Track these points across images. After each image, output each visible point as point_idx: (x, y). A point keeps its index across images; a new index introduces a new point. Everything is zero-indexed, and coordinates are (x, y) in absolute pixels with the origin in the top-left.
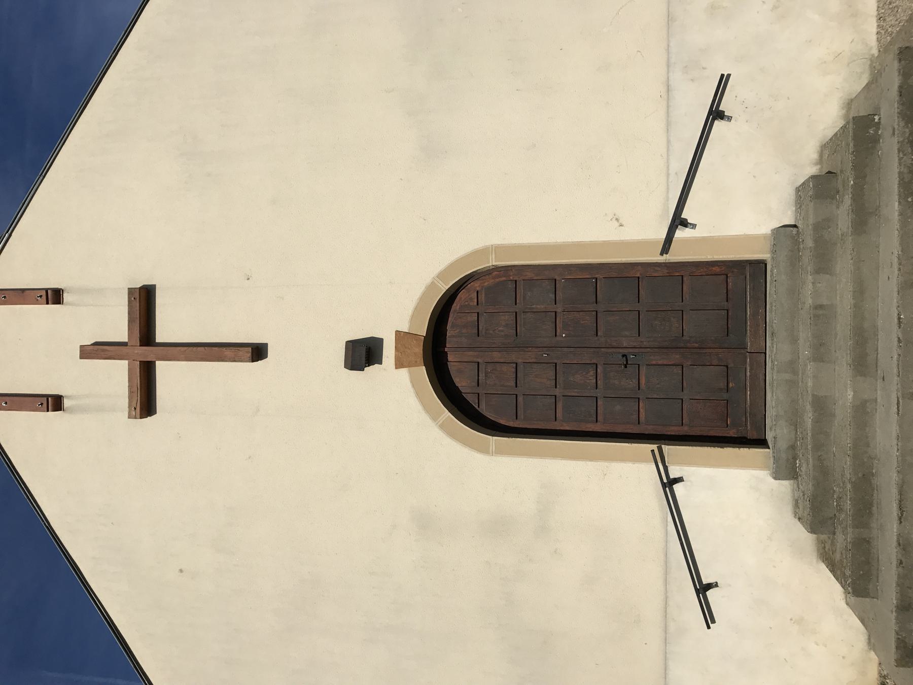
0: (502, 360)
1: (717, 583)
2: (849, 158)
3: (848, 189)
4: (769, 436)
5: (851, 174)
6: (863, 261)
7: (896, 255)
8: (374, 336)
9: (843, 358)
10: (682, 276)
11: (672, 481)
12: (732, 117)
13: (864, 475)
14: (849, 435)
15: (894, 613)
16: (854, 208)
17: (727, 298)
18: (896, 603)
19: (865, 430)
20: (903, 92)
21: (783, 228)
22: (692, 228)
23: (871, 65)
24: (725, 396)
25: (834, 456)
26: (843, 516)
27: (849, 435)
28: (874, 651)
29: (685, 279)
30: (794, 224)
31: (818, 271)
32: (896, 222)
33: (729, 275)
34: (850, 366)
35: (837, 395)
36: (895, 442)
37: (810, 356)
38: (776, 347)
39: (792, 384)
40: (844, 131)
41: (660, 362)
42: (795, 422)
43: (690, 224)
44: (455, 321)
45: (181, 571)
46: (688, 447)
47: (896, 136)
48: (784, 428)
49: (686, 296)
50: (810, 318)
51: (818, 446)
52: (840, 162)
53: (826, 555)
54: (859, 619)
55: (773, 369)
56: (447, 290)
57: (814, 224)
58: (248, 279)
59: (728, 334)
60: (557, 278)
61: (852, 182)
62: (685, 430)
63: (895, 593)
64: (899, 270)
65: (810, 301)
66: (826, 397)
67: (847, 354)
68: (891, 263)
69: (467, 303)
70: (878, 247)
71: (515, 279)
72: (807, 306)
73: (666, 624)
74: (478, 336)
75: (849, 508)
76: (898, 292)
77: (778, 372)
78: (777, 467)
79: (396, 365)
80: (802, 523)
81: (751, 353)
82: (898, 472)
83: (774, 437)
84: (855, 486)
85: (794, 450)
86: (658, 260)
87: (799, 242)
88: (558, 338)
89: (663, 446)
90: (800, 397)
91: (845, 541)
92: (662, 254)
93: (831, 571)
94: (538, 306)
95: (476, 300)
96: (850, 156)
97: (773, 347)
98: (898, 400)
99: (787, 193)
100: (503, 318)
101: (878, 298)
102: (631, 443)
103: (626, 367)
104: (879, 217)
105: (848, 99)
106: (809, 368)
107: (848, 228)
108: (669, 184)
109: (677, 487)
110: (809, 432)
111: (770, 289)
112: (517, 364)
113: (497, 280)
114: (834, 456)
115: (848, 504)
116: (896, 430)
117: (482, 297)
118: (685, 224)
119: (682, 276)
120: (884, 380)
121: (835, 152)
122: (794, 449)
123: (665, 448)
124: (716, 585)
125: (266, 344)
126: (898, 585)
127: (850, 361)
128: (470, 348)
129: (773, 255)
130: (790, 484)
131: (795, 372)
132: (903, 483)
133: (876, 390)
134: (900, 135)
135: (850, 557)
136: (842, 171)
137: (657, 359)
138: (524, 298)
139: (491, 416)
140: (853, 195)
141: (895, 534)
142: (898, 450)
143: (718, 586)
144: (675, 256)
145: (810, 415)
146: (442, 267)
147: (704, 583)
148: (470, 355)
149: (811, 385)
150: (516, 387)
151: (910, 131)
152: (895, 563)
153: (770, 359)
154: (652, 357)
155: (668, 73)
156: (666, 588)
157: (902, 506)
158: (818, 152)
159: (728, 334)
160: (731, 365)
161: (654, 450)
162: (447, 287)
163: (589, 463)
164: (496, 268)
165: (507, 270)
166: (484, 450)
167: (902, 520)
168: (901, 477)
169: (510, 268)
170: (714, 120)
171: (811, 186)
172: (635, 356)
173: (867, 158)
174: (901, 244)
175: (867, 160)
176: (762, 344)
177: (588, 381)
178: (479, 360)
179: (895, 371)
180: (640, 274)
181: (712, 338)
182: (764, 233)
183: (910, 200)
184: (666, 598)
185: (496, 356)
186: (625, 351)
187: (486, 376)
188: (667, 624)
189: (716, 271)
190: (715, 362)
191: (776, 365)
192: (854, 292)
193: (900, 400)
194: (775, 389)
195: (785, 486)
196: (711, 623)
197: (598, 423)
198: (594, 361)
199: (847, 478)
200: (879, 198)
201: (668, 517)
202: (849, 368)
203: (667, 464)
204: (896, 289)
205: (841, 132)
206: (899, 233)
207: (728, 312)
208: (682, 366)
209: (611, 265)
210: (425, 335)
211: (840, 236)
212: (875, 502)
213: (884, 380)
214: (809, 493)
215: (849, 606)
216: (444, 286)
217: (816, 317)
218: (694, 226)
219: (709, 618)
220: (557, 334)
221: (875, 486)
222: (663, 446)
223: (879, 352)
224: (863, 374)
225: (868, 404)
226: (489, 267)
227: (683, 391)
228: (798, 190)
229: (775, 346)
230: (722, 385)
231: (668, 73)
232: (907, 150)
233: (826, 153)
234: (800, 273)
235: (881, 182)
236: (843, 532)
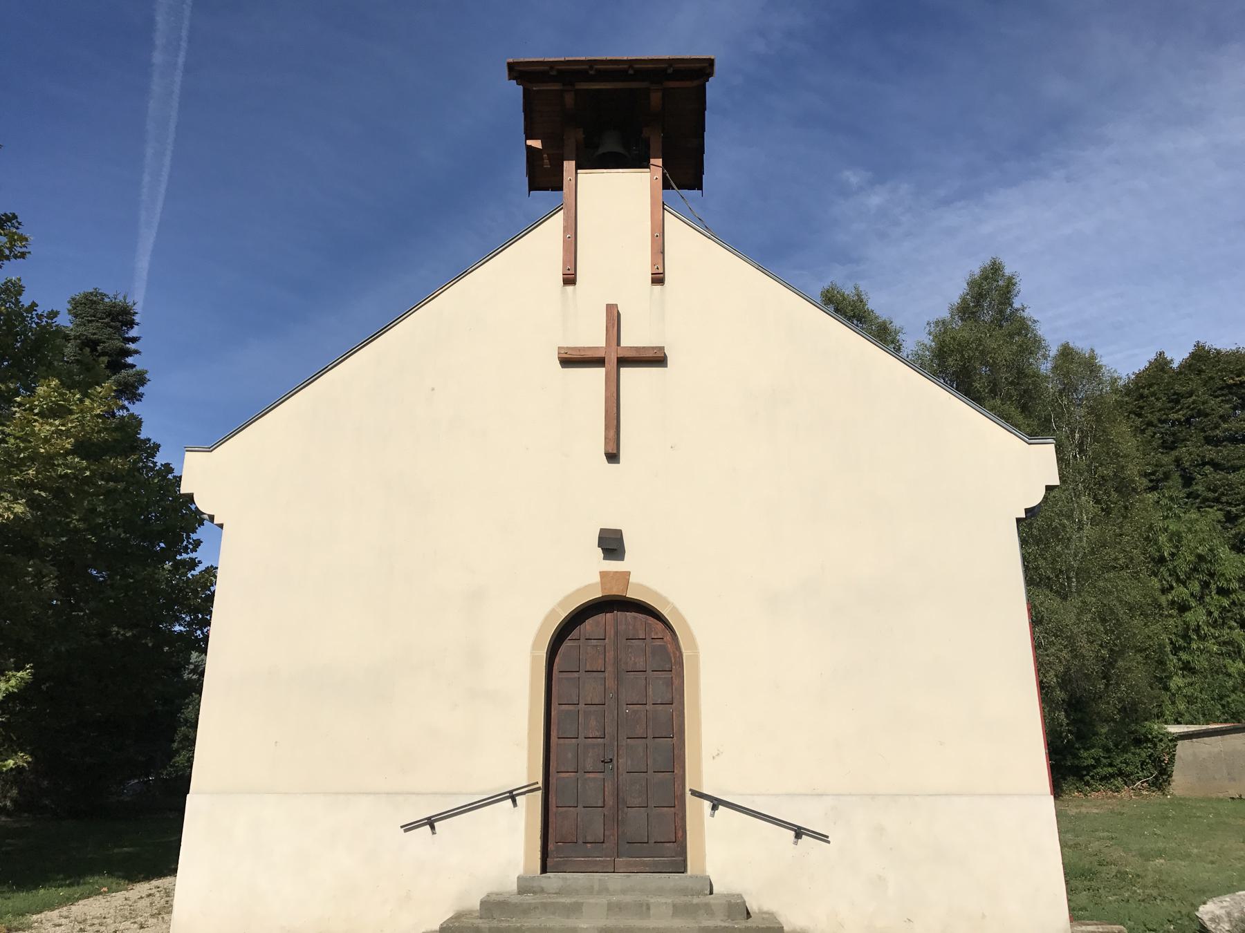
0: (607, 659)
24: (580, 841)
29: (672, 809)
30: (715, 891)
41: (606, 789)
45: (433, 389)
51: (545, 906)
62: (553, 809)
72: (649, 899)
77: (600, 880)
88: (625, 706)
89: (541, 791)
92: (690, 790)
100: (642, 660)
103: (602, 762)
113: (672, 655)
117: (658, 643)
118: (714, 808)
123: (539, 794)
124: (434, 833)
128: (616, 633)
137: (609, 787)
148: (611, 632)
154: (610, 783)
160: (604, 845)
166: (535, 646)
170: (795, 831)
185: (610, 655)
186: (615, 761)
187: (594, 646)
195: (514, 887)
217: (641, 905)
218: (712, 816)
219: (408, 827)
222: (541, 791)
230: (589, 839)
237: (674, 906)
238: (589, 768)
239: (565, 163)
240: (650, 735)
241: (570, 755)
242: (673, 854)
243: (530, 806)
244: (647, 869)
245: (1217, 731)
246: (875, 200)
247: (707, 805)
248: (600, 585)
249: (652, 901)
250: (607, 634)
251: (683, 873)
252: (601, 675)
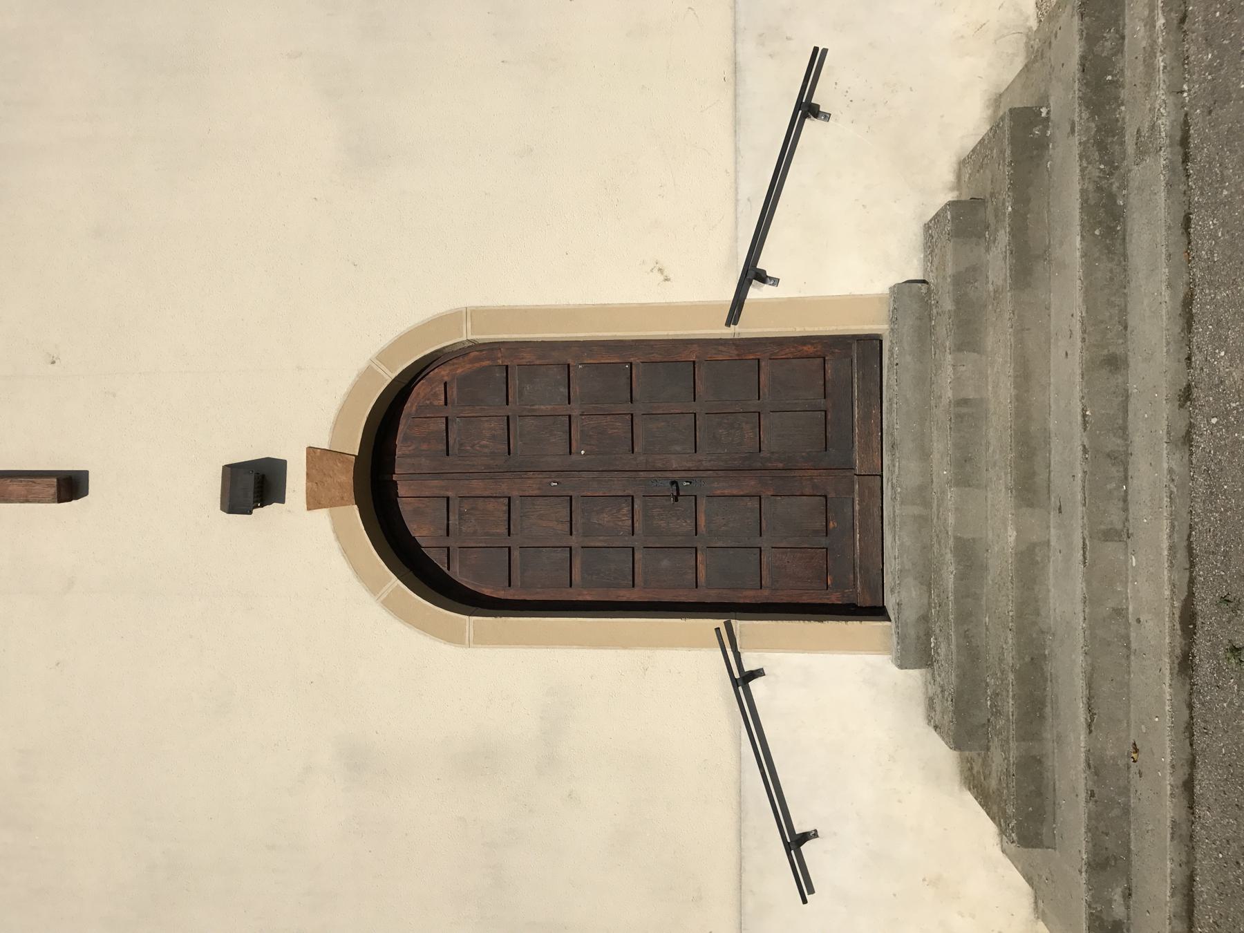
0: (486, 494)
1: (816, 831)
2: (1004, 172)
3: (1004, 221)
4: (890, 602)
5: (1009, 196)
6: (1028, 329)
7: (1078, 318)
8: (270, 457)
9: (1000, 479)
10: (759, 360)
11: (746, 676)
12: (830, 115)
13: (1032, 659)
14: (1010, 597)
15: (1083, 874)
16: (1014, 248)
17: (825, 393)
18: (1087, 858)
19: (1033, 589)
20: (1087, 65)
21: (907, 284)
22: (773, 285)
23: (1027, 43)
24: (824, 541)
25: (987, 629)
26: (1002, 722)
27: (1010, 597)
28: (1043, 921)
29: (763, 364)
30: (920, 277)
31: (959, 348)
32: (1078, 266)
33: (827, 358)
34: (1011, 492)
35: (990, 535)
36: (1079, 607)
37: (950, 478)
38: (899, 465)
39: (923, 521)
40: (996, 132)
41: (726, 492)
42: (928, 578)
43: (771, 278)
44: (408, 431)
46: (770, 622)
47: (1076, 134)
48: (913, 589)
49: (765, 390)
50: (950, 420)
51: (965, 617)
52: (990, 181)
53: (974, 780)
54: (1024, 877)
55: (894, 499)
56: (394, 380)
57: (954, 276)
58: (53, 362)
59: (826, 448)
60: (572, 363)
61: (1010, 209)
62: (764, 596)
63: (1084, 842)
64: (1083, 340)
65: (950, 394)
66: (973, 539)
67: (1006, 474)
68: (1071, 331)
69: (428, 402)
70: (1048, 308)
71: (506, 364)
72: (945, 401)
73: (741, 901)
74: (448, 455)
75: (1011, 710)
76: (1083, 375)
77: (902, 503)
78: (902, 649)
79: (308, 503)
80: (941, 734)
81: (860, 475)
82: (1086, 653)
83: (898, 604)
84: (1022, 679)
85: (928, 622)
86: (722, 334)
87: (931, 305)
88: (574, 457)
89: (733, 621)
90: (935, 540)
91: (1006, 761)
92: (728, 324)
93: (982, 806)
94: (542, 407)
95: (443, 397)
96: (1007, 169)
97: (894, 466)
98: (1084, 544)
99: (913, 233)
100: (486, 425)
101: (1049, 386)
102: (685, 617)
103: (676, 500)
104: (1050, 262)
105: (996, 94)
106: (949, 497)
107: (1005, 280)
108: (739, 215)
109: (753, 685)
110: (950, 594)
111: (889, 379)
112: (509, 498)
113: (477, 365)
114: (987, 629)
115: (1010, 705)
116: (1082, 588)
117: (454, 393)
118: (762, 277)
119: (759, 360)
120: (1060, 512)
121: (981, 167)
122: (926, 621)
123: (737, 625)
125: (86, 473)
126: (1089, 830)
127: (1011, 484)
128: (437, 475)
129: (892, 326)
130: (921, 675)
131: (926, 504)
132: (1092, 669)
133: (1048, 527)
134: (1082, 132)
135: (1013, 787)
136: (992, 195)
137: (722, 487)
138: (521, 393)
139: (467, 582)
140: (1012, 229)
141: (1083, 750)
142: (1085, 619)
143: (818, 837)
144: (747, 328)
145: (952, 568)
147: (797, 833)
148: (435, 486)
149: (953, 523)
150: (509, 535)
151: (1096, 126)
152: (1083, 795)
153: (890, 484)
154: (715, 485)
155: (735, 43)
156: (741, 844)
157: (1092, 706)
158: (955, 171)
159: (826, 448)
160: (831, 495)
161: (719, 628)
162: (394, 375)
163: (622, 652)
164: (475, 346)
165: (492, 349)
166: (455, 638)
167: (1093, 728)
168: (1089, 662)
169: (497, 346)
170: (804, 117)
171: (949, 218)
172: (691, 483)
173: (1030, 172)
174: (1085, 301)
175: (1031, 175)
176: (876, 461)
177: (620, 523)
178: (450, 494)
179: (1079, 497)
180: (696, 357)
181: (804, 454)
182: (880, 293)
183: (1097, 232)
184: (741, 859)
185: (478, 486)
186: (676, 476)
187: (460, 519)
188: (743, 864)
189: (807, 351)
190: (807, 491)
191: (900, 493)
192: (1016, 377)
193: (1087, 542)
194: (897, 530)
195: (915, 676)
196: (809, 894)
197: (636, 589)
199: (1008, 664)
200: (1048, 233)
201: (742, 733)
202: (1010, 495)
203: (739, 650)
204: (1079, 371)
205: (991, 135)
206: (1082, 284)
207: (826, 414)
208: (760, 496)
209: (652, 343)
210: (357, 454)
211: (992, 294)
212: (1048, 700)
213: (1060, 512)
214: (951, 689)
215: (1007, 855)
216: (389, 373)
217: (960, 417)
218: (776, 281)
219: (805, 886)
220: (573, 451)
221: (1049, 675)
222: (733, 621)
223: (1052, 468)
224: (1031, 505)
225: (1037, 550)
226: (462, 342)
227: (761, 536)
228: (927, 227)
229: (897, 464)
230: (819, 524)
231: (735, 43)
232: (1094, 155)
233: (967, 171)
234: (933, 353)
235: (1052, 209)
236: (1002, 746)
238: (686, 526)
240: (625, 408)
241: (665, 563)
242: (848, 360)
244: (875, 411)
247: (756, 292)
249: (949, 394)
250: (437, 492)
251: (881, 342)
252: (516, 504)
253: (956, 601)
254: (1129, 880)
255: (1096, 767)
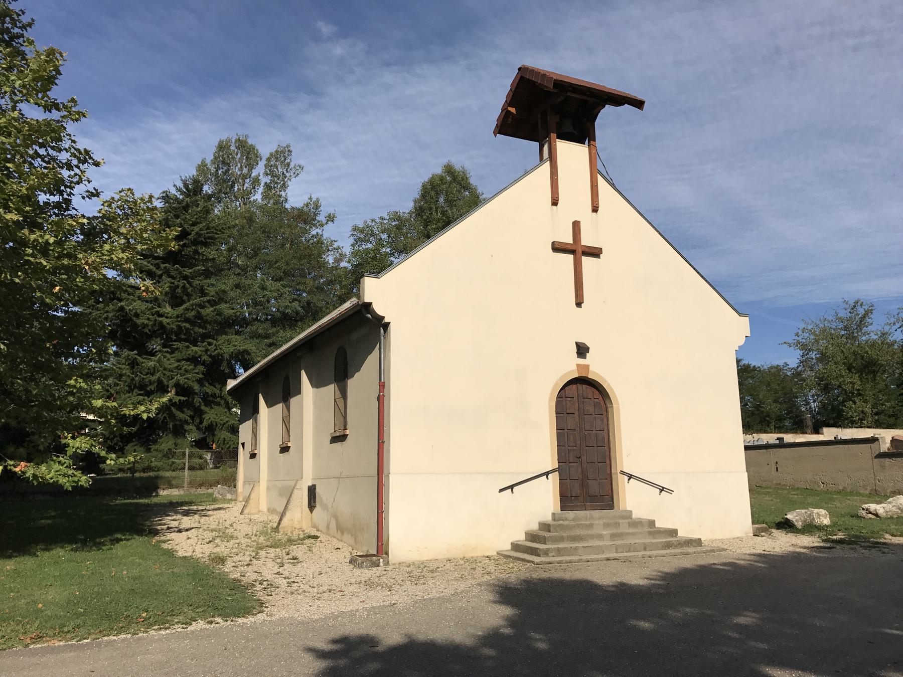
24: (570, 496)
51: (578, 525)
66: (593, 528)
117: (596, 401)
124: (512, 493)
126: (565, 547)
146: (611, 385)
166: (550, 400)
170: (660, 489)
198: (577, 445)
217: (616, 523)
219: (501, 490)
224: (611, 536)
237: (629, 523)
238: (571, 461)
239: (552, 134)
243: (555, 478)
245: (750, 448)
246: (338, 50)
247: (626, 478)
248: (577, 371)
253: (581, 524)
254: (557, 556)
255: (576, 548)
